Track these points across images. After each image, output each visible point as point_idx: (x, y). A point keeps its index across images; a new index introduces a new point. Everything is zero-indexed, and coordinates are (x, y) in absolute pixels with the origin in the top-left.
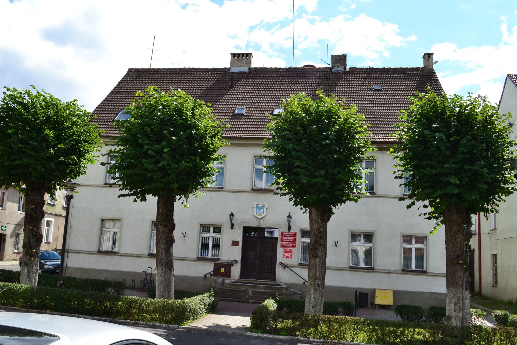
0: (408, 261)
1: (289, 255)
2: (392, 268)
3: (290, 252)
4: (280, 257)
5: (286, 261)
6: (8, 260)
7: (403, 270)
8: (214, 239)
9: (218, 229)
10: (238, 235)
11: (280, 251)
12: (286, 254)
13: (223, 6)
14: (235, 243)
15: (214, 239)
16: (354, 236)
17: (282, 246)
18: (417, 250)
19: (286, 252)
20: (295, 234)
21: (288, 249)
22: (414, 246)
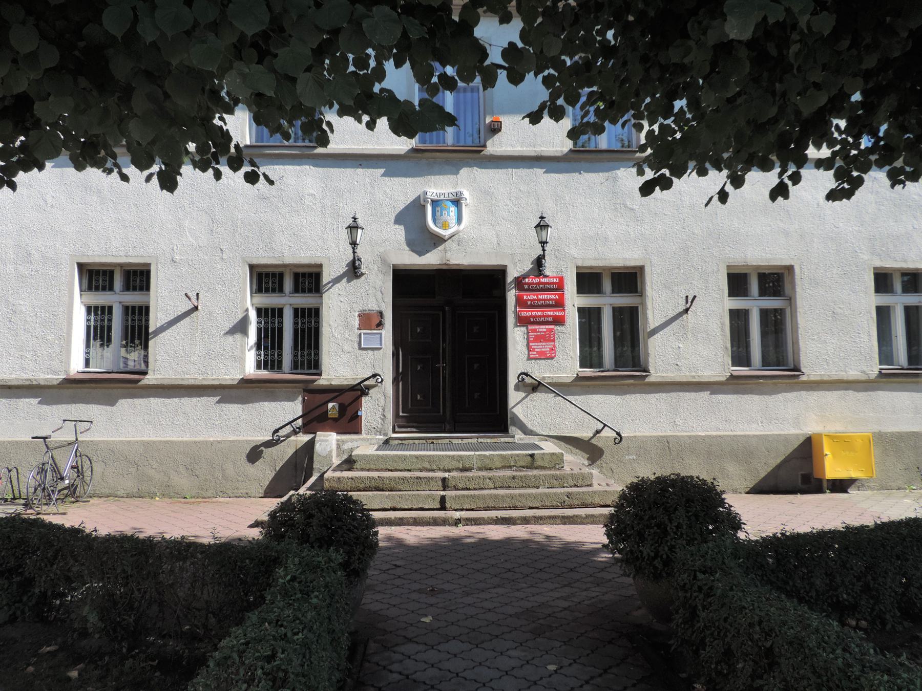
0: (591, 347)
1: (545, 347)
2: (853, 373)
3: (549, 338)
4: (518, 357)
5: (541, 371)
6: (362, 469)
7: (881, 374)
8: (128, 310)
9: (309, 279)
10: (377, 293)
11: (516, 337)
12: (537, 347)
13: (505, 25)
14: (370, 321)
15: (128, 310)
16: (737, 283)
17: (522, 321)
18: (764, 313)
19: (538, 339)
20: (559, 287)
21: (543, 328)
22: (288, 301)
